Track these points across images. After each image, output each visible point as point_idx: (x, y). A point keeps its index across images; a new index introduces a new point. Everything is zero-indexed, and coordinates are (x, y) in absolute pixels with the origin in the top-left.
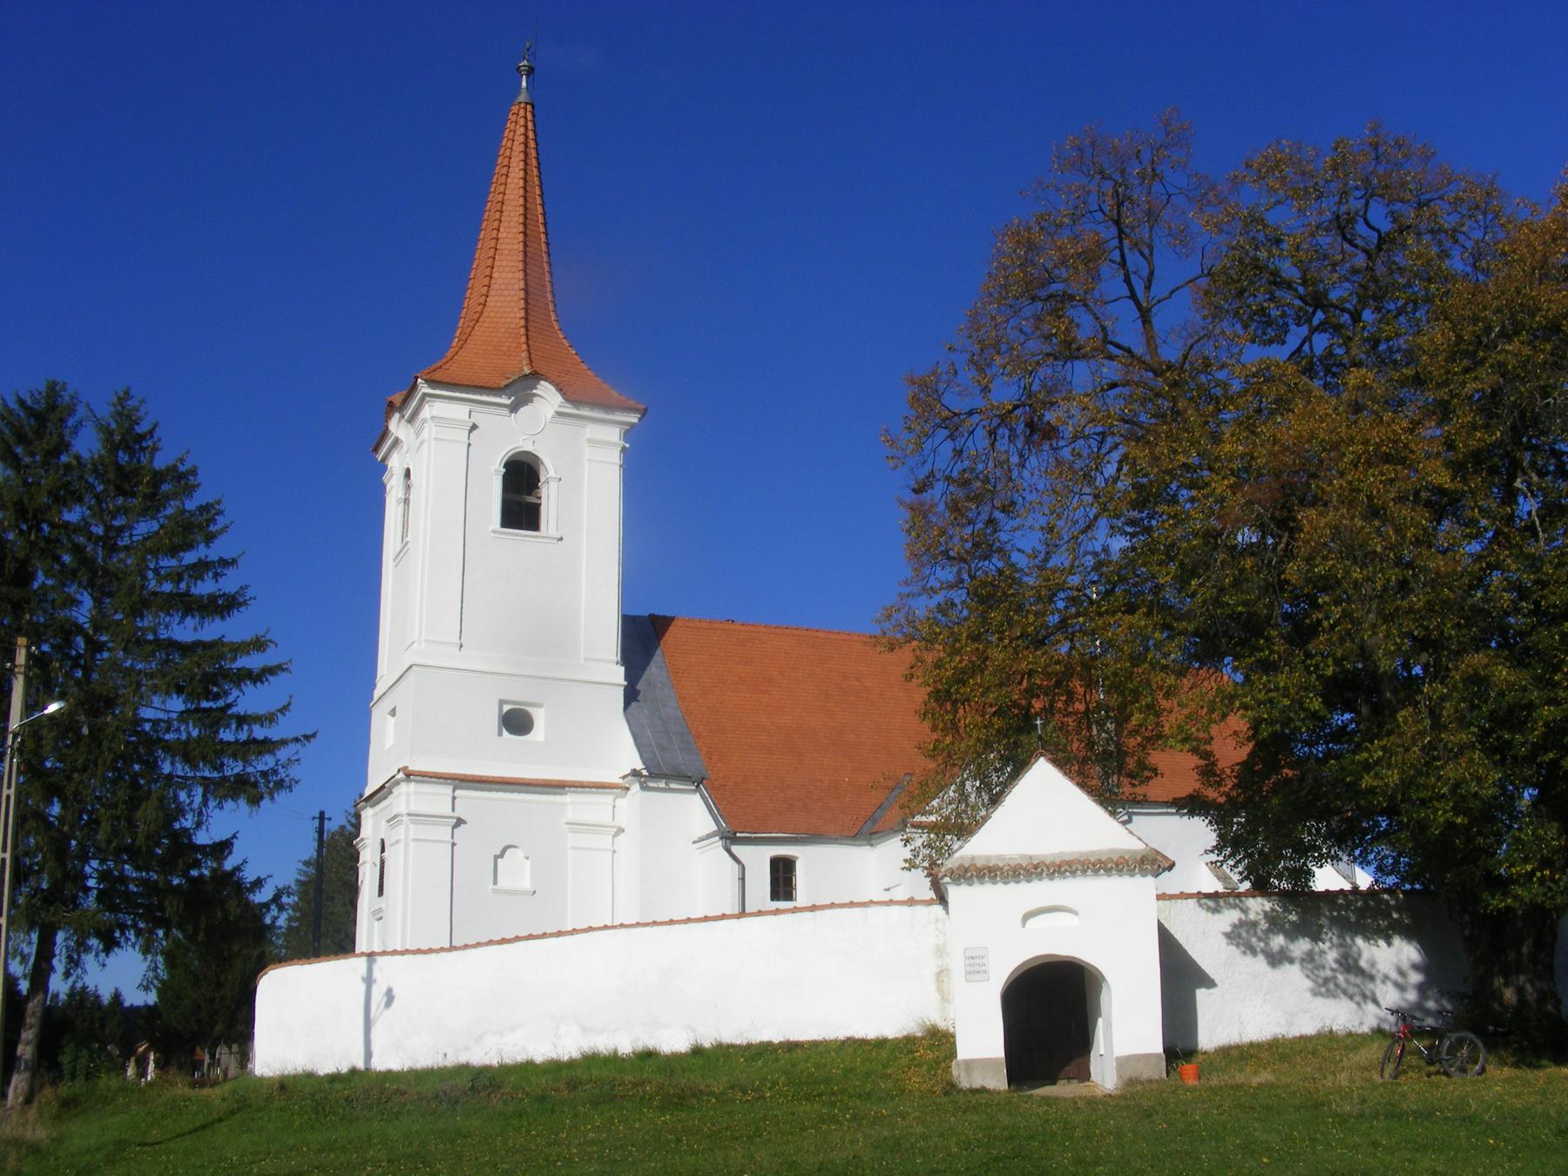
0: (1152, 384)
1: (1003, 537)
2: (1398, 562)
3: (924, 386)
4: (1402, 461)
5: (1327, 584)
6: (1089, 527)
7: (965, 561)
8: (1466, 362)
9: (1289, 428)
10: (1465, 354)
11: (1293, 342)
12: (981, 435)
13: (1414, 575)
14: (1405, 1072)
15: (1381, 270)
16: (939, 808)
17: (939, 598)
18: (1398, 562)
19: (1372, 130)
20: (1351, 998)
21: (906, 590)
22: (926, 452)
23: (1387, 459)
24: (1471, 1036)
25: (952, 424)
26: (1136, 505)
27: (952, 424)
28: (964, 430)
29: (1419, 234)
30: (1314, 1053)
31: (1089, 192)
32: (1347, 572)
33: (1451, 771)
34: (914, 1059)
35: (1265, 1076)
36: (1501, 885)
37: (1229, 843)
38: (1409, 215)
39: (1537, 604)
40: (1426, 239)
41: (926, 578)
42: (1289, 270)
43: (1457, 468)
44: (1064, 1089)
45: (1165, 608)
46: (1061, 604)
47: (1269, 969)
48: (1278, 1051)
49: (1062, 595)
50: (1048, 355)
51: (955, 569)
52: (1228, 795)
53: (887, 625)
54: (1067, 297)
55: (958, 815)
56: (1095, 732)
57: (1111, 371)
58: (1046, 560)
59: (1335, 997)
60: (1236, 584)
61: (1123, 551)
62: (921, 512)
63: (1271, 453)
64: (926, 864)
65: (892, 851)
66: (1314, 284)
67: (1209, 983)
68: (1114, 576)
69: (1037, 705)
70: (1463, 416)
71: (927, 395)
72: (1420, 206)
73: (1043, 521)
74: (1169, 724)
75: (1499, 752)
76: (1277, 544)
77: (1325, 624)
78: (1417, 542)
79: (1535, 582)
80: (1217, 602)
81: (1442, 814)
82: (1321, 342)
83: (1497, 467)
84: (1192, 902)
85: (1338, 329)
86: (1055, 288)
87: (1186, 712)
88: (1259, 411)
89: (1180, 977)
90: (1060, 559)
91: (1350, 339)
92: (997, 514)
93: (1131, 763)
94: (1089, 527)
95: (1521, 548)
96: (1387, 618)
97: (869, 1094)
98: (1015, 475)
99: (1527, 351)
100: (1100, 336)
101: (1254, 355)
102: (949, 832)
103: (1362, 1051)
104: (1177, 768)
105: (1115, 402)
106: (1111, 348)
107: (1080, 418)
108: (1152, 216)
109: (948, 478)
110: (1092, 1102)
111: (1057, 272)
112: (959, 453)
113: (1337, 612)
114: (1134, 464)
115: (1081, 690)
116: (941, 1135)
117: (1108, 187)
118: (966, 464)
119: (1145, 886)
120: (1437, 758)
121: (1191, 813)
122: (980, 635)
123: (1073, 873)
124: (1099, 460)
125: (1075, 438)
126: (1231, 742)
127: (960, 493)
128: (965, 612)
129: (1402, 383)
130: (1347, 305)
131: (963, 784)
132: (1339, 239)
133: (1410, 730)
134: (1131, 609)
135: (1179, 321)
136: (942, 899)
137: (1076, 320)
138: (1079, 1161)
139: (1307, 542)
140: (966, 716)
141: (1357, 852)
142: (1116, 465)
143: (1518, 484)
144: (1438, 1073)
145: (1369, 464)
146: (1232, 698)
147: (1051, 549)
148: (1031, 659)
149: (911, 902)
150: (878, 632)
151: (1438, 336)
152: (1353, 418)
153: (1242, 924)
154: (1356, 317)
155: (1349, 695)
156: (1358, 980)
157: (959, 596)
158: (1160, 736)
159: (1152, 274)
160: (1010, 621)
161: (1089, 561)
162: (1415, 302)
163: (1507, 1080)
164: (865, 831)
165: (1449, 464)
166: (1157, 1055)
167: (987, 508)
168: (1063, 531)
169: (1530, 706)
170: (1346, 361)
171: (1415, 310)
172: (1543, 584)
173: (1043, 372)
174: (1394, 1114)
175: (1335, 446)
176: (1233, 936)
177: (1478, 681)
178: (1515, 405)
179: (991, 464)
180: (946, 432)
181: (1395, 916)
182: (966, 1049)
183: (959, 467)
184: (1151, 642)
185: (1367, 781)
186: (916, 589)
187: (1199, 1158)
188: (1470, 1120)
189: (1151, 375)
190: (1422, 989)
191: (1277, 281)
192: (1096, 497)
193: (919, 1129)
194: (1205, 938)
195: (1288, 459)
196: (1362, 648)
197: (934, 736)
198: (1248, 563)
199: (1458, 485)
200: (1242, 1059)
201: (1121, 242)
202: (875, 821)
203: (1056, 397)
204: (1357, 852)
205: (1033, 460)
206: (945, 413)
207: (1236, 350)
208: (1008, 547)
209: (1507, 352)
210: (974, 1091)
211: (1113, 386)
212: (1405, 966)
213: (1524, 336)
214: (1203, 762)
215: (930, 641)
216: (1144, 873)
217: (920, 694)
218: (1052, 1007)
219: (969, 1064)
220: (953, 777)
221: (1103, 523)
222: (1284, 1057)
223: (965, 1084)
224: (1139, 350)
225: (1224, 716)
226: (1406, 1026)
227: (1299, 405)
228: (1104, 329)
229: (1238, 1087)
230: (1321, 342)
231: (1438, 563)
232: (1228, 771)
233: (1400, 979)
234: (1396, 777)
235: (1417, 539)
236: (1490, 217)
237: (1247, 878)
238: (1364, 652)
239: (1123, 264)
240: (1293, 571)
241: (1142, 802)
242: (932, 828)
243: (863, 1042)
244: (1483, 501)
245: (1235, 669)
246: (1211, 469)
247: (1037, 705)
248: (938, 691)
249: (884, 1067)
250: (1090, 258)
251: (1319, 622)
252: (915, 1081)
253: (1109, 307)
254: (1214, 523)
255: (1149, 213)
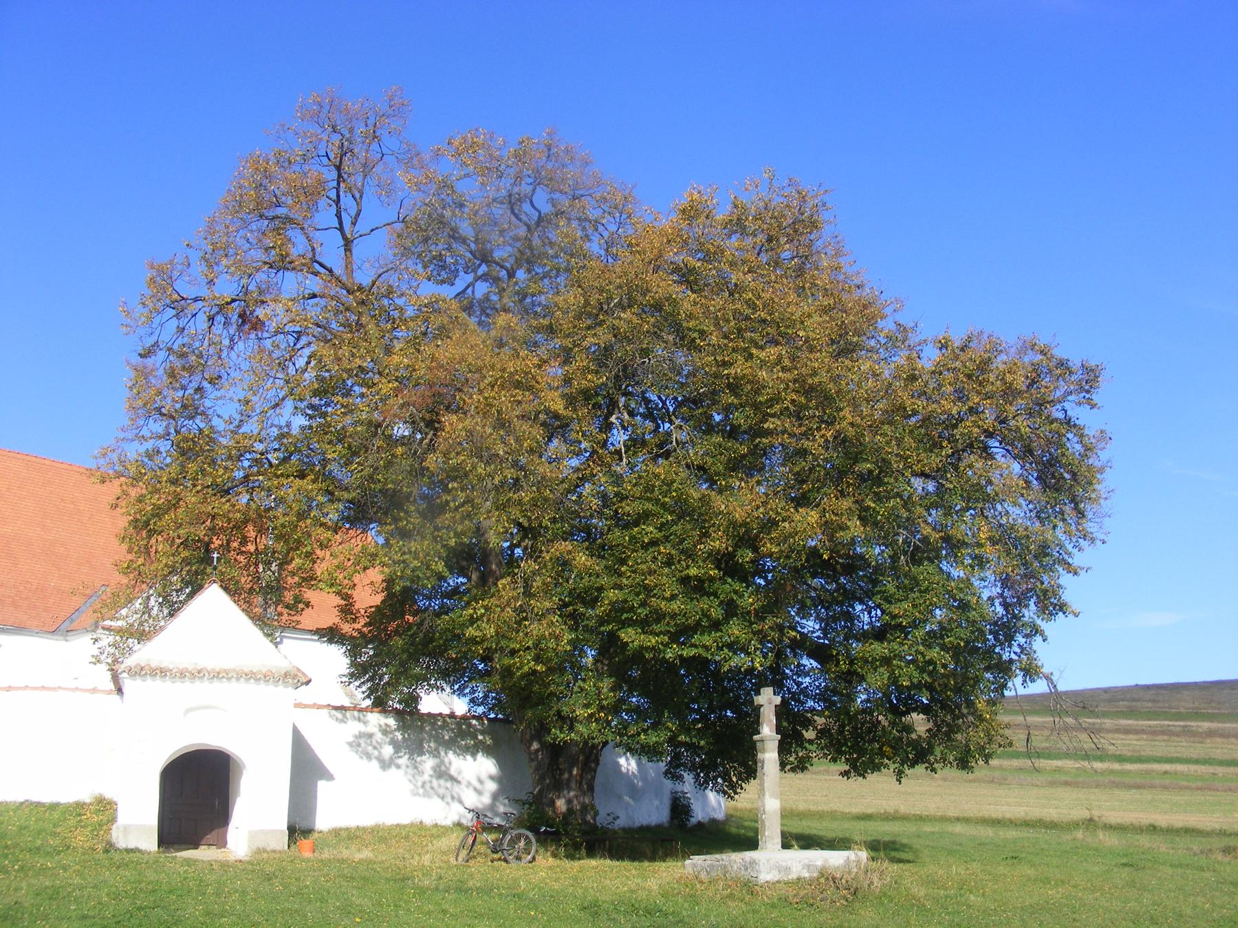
0: (344, 299)
1: (208, 403)
2: (515, 464)
3: (161, 271)
4: (530, 388)
5: (458, 474)
6: (277, 405)
7: (174, 418)
8: (589, 322)
9: (446, 351)
10: (590, 315)
11: (460, 285)
12: (202, 319)
13: (525, 476)
14: (475, 857)
15: (536, 242)
16: (128, 616)
17: (149, 445)
18: (515, 464)
19: (548, 134)
20: (443, 798)
21: (122, 435)
22: (154, 326)
23: (518, 385)
24: (530, 835)
25: (179, 305)
26: (316, 393)
27: (179, 305)
28: (189, 312)
29: (569, 219)
30: (407, 838)
31: (321, 140)
32: (474, 467)
33: (535, 629)
34: (81, 821)
35: (366, 854)
36: (569, 722)
37: (359, 671)
38: (565, 203)
39: (616, 512)
40: (574, 224)
41: (140, 428)
42: (466, 229)
43: (570, 401)
44: (203, 853)
45: (328, 477)
46: (246, 464)
47: (380, 771)
48: (379, 835)
49: (248, 456)
50: (265, 263)
51: (165, 424)
52: (359, 631)
53: (102, 461)
54: (288, 220)
55: (141, 624)
56: (261, 570)
57: (313, 284)
58: (239, 427)
59: (429, 797)
60: (389, 464)
61: (303, 428)
62: (144, 374)
63: (430, 369)
64: (109, 660)
65: (82, 647)
66: (483, 243)
67: (330, 777)
68: (291, 448)
69: (217, 543)
70: (580, 361)
71: (162, 279)
72: (574, 198)
73: (241, 395)
74: (320, 569)
75: (574, 620)
76: (422, 440)
77: (452, 504)
78: (531, 451)
79: (616, 495)
80: (371, 478)
81: (527, 663)
82: (481, 289)
83: (600, 405)
84: (326, 711)
85: (496, 280)
86: (280, 211)
87: (336, 562)
88: (425, 334)
89: (306, 770)
90: (251, 427)
91: (504, 290)
92: (205, 384)
93: (289, 597)
94: (277, 405)
95: (610, 466)
96: (502, 507)
97: (38, 849)
98: (224, 355)
99: (636, 320)
100: (310, 255)
101: (428, 290)
102: (131, 635)
103: (444, 839)
104: (323, 607)
105: (314, 310)
106: (317, 266)
107: (283, 318)
108: (367, 168)
109: (169, 349)
110: (225, 865)
111: (284, 198)
112: (181, 330)
113: (462, 496)
114: (320, 361)
115: (253, 534)
116: (95, 887)
117: (336, 138)
118: (186, 340)
119: (288, 694)
120: (526, 619)
121: (330, 641)
122: (177, 480)
123: (229, 679)
124: (294, 351)
125: (277, 333)
126: (369, 590)
127: (178, 364)
128: (169, 460)
129: (538, 330)
130: (508, 265)
131: (148, 598)
132: (509, 212)
133: (507, 594)
134: (302, 475)
135: (374, 255)
136: (120, 690)
137: (293, 239)
138: (208, 913)
139: (446, 439)
140: (159, 544)
141: (456, 687)
142: (306, 359)
143: (613, 419)
144: (500, 859)
145: (502, 387)
146: (374, 556)
147: (245, 417)
148: (220, 505)
149: (94, 690)
150: (94, 467)
151: (571, 298)
152: (497, 350)
153: (361, 735)
154: (511, 274)
155: (464, 563)
156: (449, 784)
157: (165, 446)
158: (312, 578)
159: (358, 214)
160: (203, 470)
161: (275, 432)
162: (558, 270)
163: (550, 868)
164: (61, 628)
165: (563, 396)
166: (282, 831)
167: (197, 378)
168: (253, 403)
169: (600, 589)
170: (498, 306)
171: (557, 276)
172: (622, 498)
173: (261, 277)
174: (461, 889)
175: (479, 370)
176: (354, 745)
177: (564, 564)
178: (621, 360)
179: (206, 343)
180: (174, 312)
181: (480, 737)
182: (124, 817)
183: (180, 341)
184: (314, 503)
185: (471, 632)
186: (130, 436)
187: (305, 916)
188: (519, 896)
189: (345, 292)
190: (495, 797)
191: (455, 235)
192: (287, 382)
193: (77, 880)
194: (331, 741)
195: (441, 374)
196: (478, 529)
197: (130, 557)
198: (400, 450)
199: (568, 413)
200: (349, 838)
201: (339, 184)
202: (72, 621)
203: (268, 298)
204: (456, 687)
205: (241, 344)
206: (175, 296)
207: (415, 284)
208: (210, 412)
209: (620, 319)
210: (128, 851)
211: (314, 296)
212: (484, 776)
213: (635, 309)
214: (344, 602)
215: (137, 478)
216: (286, 684)
217: (122, 521)
218: (197, 789)
219: (126, 829)
220: (142, 591)
221: (289, 405)
222: (383, 840)
223: (122, 844)
224: (338, 271)
225: (365, 569)
226: (479, 822)
227: (456, 335)
228: (313, 249)
229: (343, 861)
230: (481, 289)
231: (544, 469)
232: (362, 612)
233: (478, 786)
234: (492, 630)
235: (532, 450)
236: (624, 216)
237: (368, 697)
238: (479, 531)
239: (338, 201)
240: (433, 461)
241: (294, 627)
242: (119, 631)
243: (39, 804)
244: (585, 424)
245: (379, 533)
246: (380, 373)
247: (217, 543)
248: (137, 520)
249: (55, 826)
250: (311, 194)
251: (447, 502)
252: (80, 839)
253: (318, 233)
254: (376, 416)
255: (365, 165)
